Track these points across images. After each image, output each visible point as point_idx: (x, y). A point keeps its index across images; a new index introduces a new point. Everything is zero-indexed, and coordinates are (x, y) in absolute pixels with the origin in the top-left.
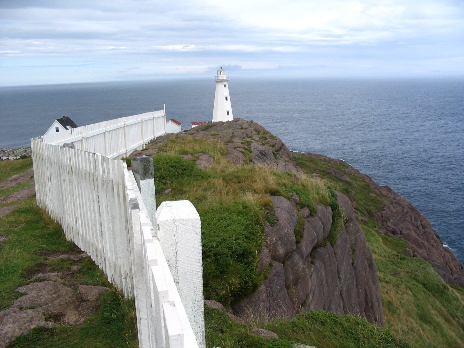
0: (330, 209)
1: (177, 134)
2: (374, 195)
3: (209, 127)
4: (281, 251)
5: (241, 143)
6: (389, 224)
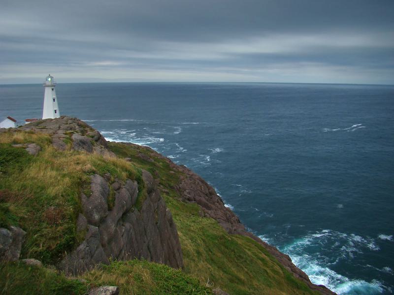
0: (136, 183)
1: (382, 234)
2: (173, 172)
3: (41, 124)
4: (97, 217)
5: (64, 134)
6: (185, 193)
